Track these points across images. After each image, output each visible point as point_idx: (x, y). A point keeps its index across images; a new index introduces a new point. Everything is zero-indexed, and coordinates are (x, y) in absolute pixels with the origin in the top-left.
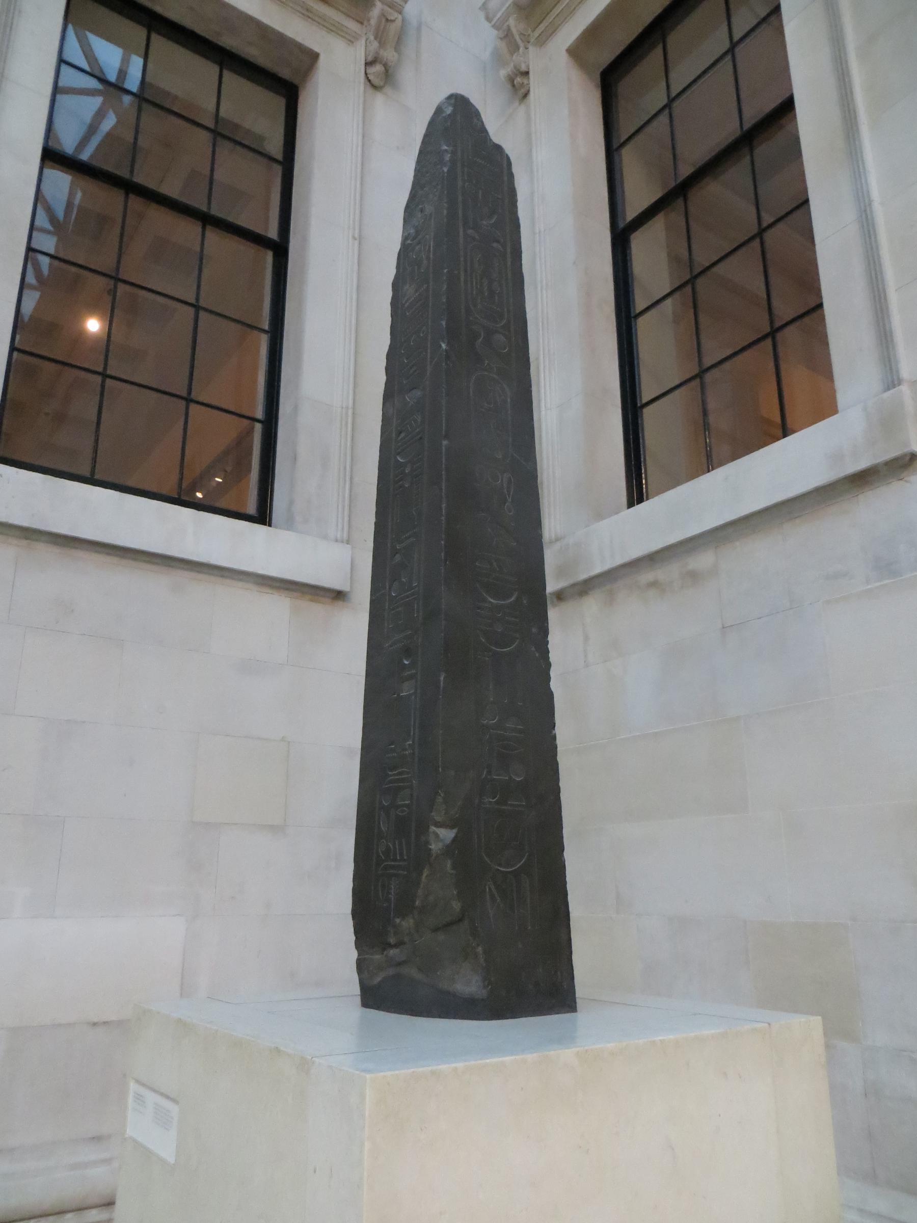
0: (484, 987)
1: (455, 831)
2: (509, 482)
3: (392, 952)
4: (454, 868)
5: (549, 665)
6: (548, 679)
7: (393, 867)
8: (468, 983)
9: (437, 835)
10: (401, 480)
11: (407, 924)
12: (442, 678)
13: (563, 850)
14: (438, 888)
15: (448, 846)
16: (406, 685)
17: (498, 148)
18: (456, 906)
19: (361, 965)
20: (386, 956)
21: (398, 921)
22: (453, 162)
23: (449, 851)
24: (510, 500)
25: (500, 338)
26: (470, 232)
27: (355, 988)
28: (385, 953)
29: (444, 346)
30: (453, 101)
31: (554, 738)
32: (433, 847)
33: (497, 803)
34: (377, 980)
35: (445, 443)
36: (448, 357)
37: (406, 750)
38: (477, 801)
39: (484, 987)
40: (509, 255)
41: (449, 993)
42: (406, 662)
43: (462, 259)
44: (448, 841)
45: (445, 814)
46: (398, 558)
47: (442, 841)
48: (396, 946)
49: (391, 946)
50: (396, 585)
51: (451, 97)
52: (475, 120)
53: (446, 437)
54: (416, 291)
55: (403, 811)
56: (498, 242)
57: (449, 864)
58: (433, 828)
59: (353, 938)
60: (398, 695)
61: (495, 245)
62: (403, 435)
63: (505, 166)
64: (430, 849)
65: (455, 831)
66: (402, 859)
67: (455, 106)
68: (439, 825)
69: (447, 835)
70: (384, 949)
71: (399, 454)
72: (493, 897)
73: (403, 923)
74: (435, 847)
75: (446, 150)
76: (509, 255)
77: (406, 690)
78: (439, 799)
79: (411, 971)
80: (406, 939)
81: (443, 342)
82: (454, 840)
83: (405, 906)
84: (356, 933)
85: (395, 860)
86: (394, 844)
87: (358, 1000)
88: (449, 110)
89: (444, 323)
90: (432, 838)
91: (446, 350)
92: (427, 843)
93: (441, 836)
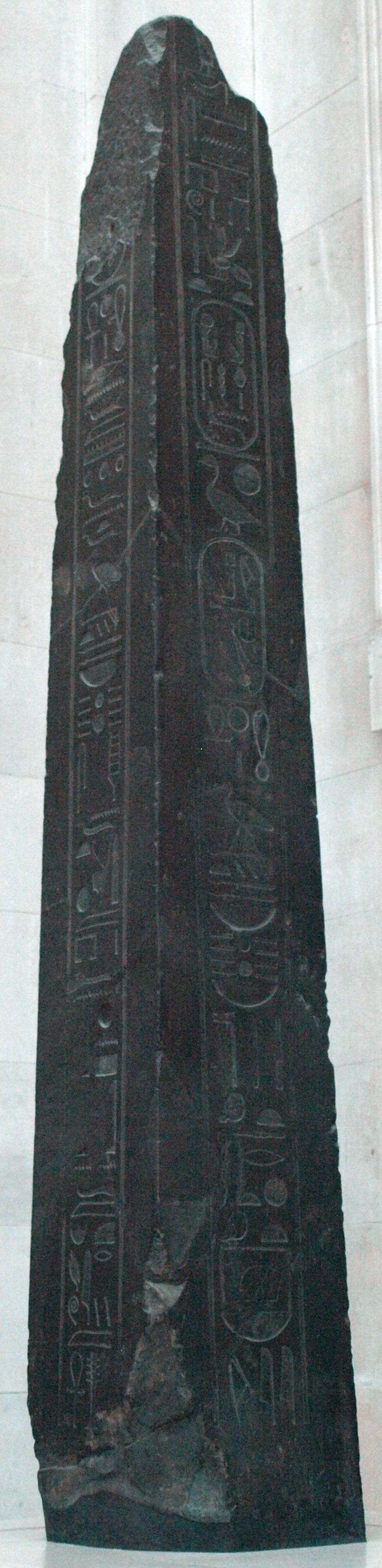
0: (229, 1506)
1: (181, 1287)
2: (263, 724)
3: (92, 1461)
4: (180, 1341)
5: (326, 1022)
6: (326, 1043)
7: (88, 1338)
8: (206, 1503)
9: (155, 1295)
10: (88, 717)
11: (114, 1419)
12: (158, 1061)
13: (347, 1308)
14: (155, 1367)
15: (171, 1312)
16: (104, 1061)
17: (245, 106)
18: (186, 1394)
19: (45, 1481)
20: (85, 1466)
21: (100, 1416)
22: (164, 155)
23: (172, 1317)
24: (263, 756)
25: (247, 471)
26: (197, 284)
27: (39, 1519)
28: (82, 1462)
29: (154, 505)
30: (163, 34)
31: (334, 1137)
32: (150, 1311)
33: (247, 1242)
34: (72, 1500)
35: (157, 676)
36: (160, 522)
37: (106, 1163)
38: (214, 1242)
39: (229, 1506)
40: (262, 312)
41: (175, 1515)
42: (104, 1026)
43: (182, 340)
44: (171, 1303)
45: (168, 1263)
46: (85, 851)
47: (160, 1301)
48: (98, 1452)
49: (89, 1452)
50: (84, 894)
51: (159, 24)
52: (204, 62)
53: (161, 665)
54: (106, 383)
55: (104, 1256)
56: (244, 289)
57: (174, 1334)
58: (150, 1284)
59: (30, 1441)
60: (92, 1076)
61: (237, 297)
62: (88, 639)
63: (256, 139)
64: (146, 1315)
65: (181, 1287)
66: (104, 1326)
67: (168, 42)
68: (157, 1279)
69: (170, 1293)
70: (80, 1457)
71: (84, 669)
72: (237, 1376)
73: (108, 1419)
74: (153, 1311)
75: (152, 135)
76: (262, 312)
77: (106, 1068)
78: (158, 1243)
79: (123, 1487)
80: (113, 1442)
81: (153, 498)
82: (181, 1300)
83: (110, 1395)
84: (35, 1434)
85: (95, 1328)
86: (92, 1305)
87: (43, 1533)
88: (156, 54)
89: (153, 464)
90: (148, 1300)
91: (158, 515)
92: (141, 1305)
93: (162, 1295)
